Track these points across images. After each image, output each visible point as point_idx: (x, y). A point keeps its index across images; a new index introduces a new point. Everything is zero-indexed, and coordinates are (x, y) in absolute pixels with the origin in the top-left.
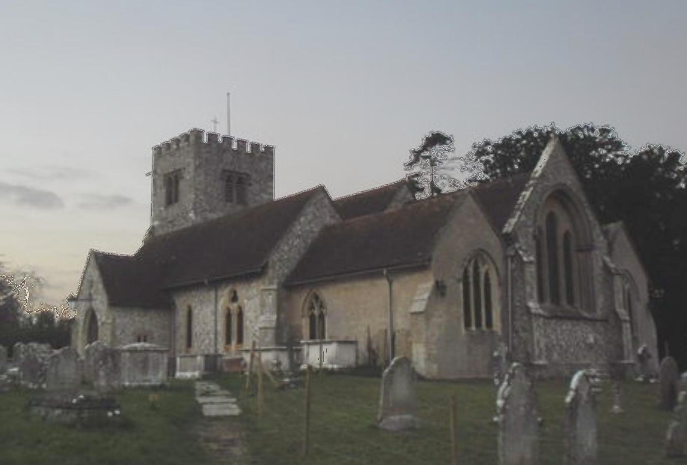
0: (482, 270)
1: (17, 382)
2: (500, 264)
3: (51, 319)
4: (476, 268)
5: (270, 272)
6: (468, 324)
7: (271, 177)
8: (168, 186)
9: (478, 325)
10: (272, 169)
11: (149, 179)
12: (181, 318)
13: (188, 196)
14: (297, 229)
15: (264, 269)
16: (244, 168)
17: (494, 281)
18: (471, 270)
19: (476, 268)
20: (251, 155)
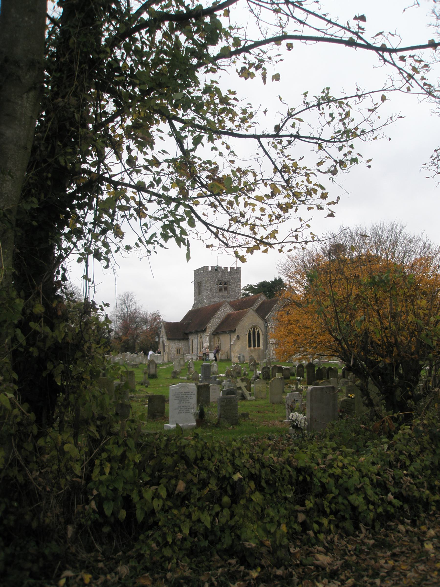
0: (256, 331)
1: (430, 441)
2: (263, 329)
3: (78, 354)
4: (254, 330)
5: (207, 330)
6: (250, 346)
7: (240, 281)
8: (199, 287)
9: (254, 346)
10: (240, 277)
11: (193, 284)
12: (190, 343)
13: (205, 293)
14: (217, 315)
15: (205, 330)
16: (227, 279)
17: (261, 334)
18: (252, 331)
19: (254, 330)
20: (230, 272)
